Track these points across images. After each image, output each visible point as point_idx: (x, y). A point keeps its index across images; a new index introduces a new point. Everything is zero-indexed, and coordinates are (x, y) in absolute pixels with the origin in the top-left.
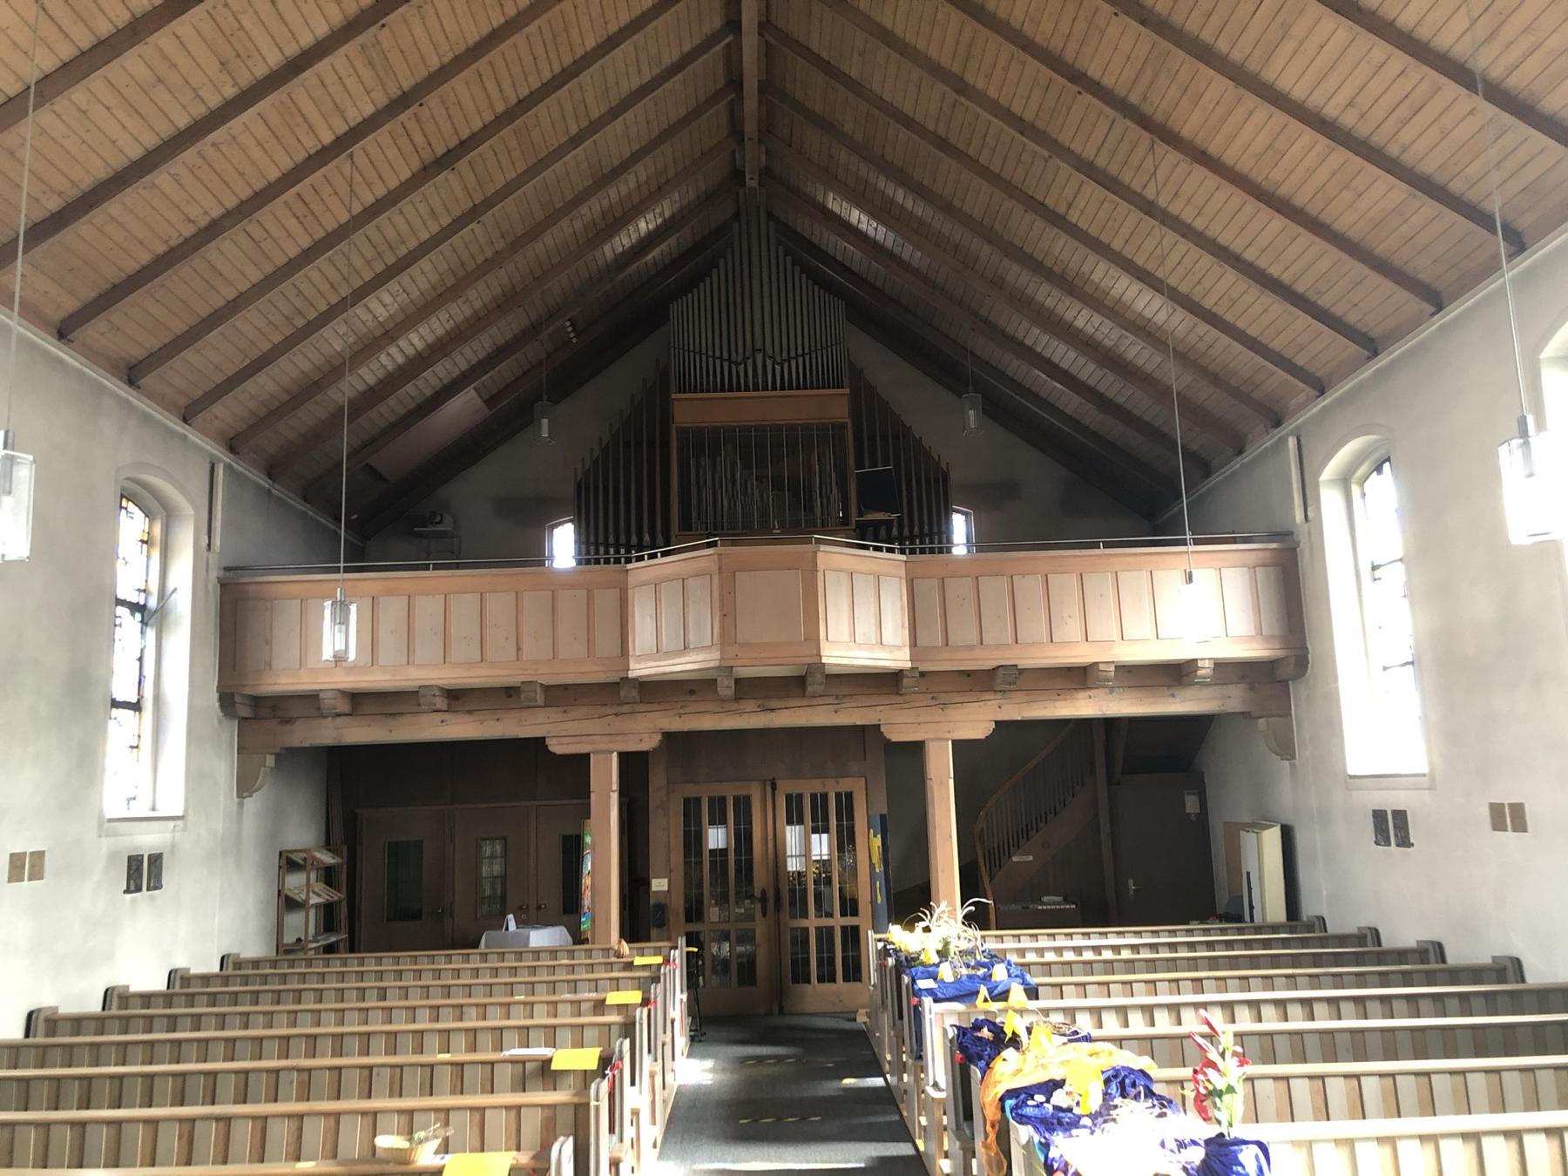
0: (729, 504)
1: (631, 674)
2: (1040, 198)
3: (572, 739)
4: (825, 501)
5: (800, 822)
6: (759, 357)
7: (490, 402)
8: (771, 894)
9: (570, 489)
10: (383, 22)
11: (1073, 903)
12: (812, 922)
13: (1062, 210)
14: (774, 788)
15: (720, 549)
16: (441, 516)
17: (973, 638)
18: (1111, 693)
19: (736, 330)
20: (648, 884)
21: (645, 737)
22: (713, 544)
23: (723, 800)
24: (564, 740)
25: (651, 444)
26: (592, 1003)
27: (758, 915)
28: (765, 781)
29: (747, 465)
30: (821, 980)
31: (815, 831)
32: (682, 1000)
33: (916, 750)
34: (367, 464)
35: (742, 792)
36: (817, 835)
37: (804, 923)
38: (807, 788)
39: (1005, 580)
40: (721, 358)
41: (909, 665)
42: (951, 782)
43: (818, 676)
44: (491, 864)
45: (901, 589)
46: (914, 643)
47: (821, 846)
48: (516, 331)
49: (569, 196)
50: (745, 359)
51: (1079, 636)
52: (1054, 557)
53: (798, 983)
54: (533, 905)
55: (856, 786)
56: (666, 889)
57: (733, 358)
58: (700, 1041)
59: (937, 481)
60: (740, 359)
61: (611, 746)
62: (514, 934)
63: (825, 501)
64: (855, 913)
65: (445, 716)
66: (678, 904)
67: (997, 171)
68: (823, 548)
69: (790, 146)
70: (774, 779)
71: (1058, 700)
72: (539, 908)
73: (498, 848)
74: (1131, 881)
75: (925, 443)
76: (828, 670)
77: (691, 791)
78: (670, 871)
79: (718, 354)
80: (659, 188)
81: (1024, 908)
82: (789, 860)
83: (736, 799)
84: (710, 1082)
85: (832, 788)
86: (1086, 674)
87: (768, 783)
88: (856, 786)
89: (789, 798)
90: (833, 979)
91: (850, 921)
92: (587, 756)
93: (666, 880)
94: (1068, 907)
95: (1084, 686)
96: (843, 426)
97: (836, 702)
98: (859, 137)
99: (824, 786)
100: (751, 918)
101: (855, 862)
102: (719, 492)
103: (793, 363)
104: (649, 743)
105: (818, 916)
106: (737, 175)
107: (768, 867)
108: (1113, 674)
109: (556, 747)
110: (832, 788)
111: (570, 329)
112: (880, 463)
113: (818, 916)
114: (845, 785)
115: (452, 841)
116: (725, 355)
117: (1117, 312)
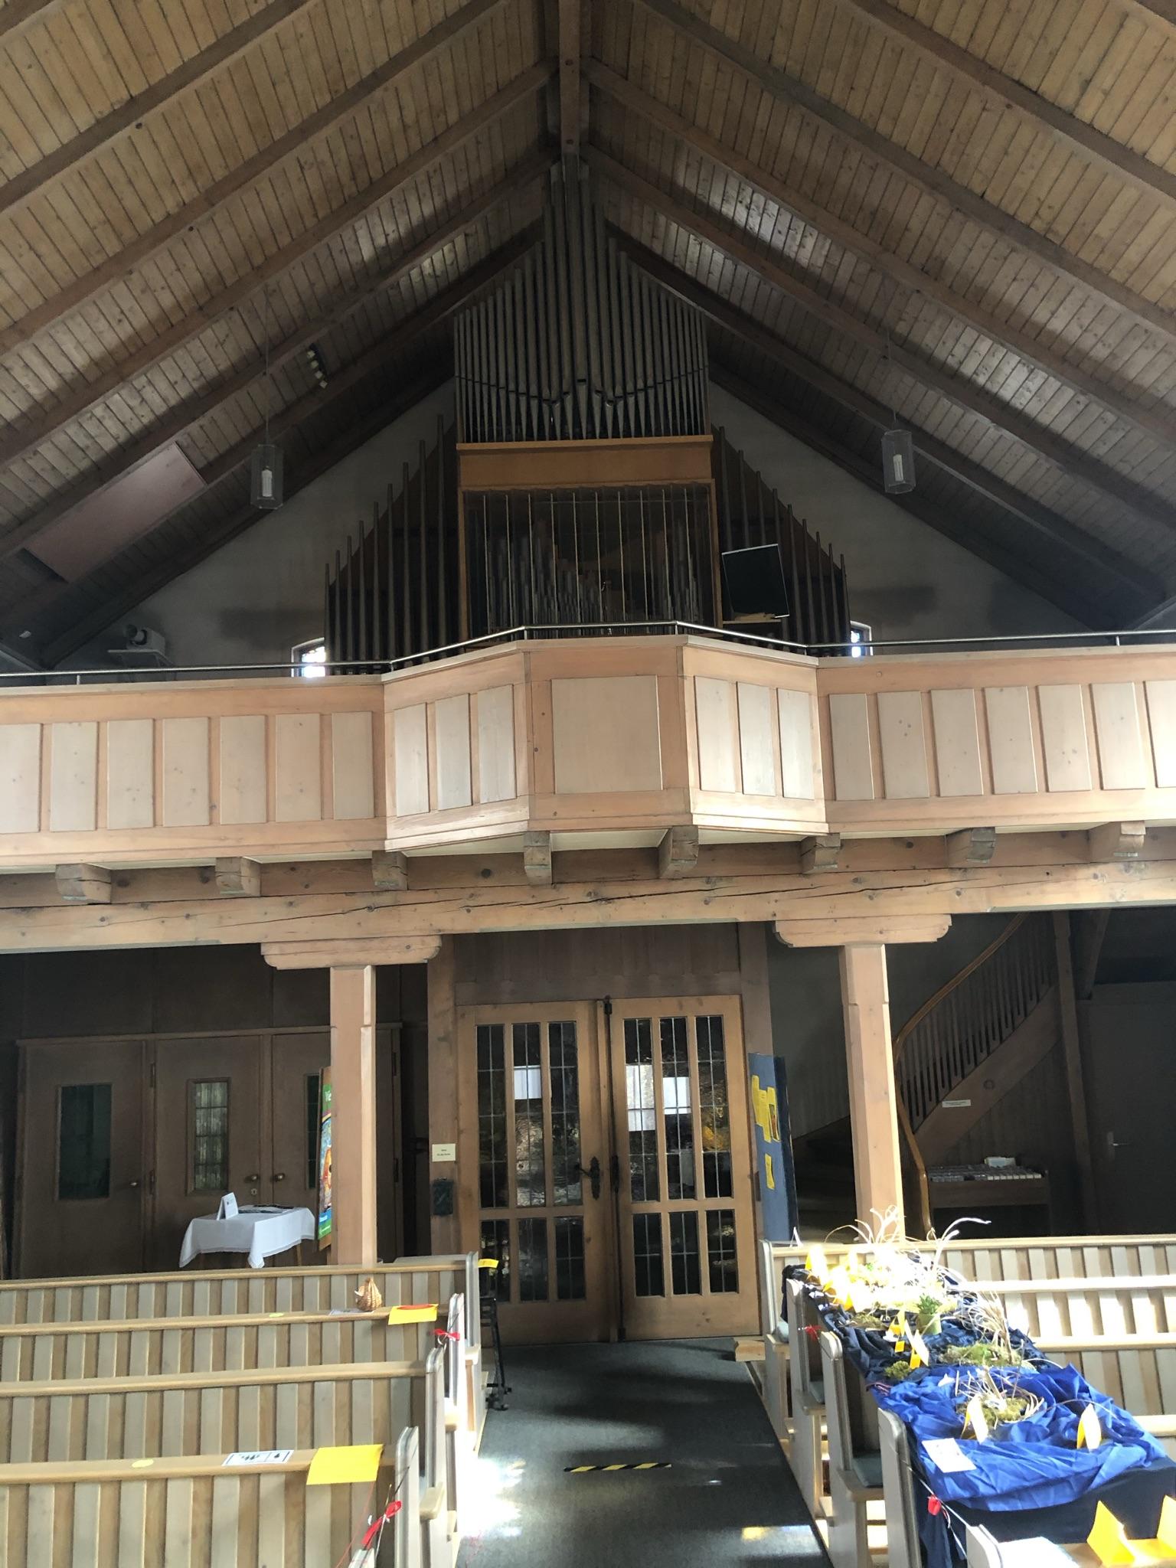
0: (541, 603)
1: (390, 846)
2: (1032, 82)
3: (308, 946)
4: (678, 600)
5: (646, 1057)
6: (582, 390)
7: (206, 471)
8: (605, 1166)
9: (318, 600)
10: (140, 120)
11: (1038, 1172)
12: (665, 1206)
13: (1067, 100)
14: (608, 1010)
15: (527, 643)
16: (145, 632)
17: (925, 788)
18: (1127, 871)
19: (546, 303)
20: (427, 1152)
21: (416, 943)
22: (520, 636)
23: (534, 1029)
24: (289, 948)
25: (432, 531)
26: (283, 1478)
27: (588, 1196)
28: (596, 1000)
29: (565, 553)
30: (679, 1290)
31: (670, 1072)
32: (469, 1364)
33: (832, 957)
34: (24, 551)
35: (561, 1017)
36: (672, 1079)
37: (653, 1207)
38: (656, 1010)
39: (973, 695)
40: (527, 394)
41: (824, 829)
42: (886, 1008)
43: (688, 847)
44: (208, 1116)
45: (811, 711)
46: (832, 794)
47: (678, 1095)
48: (234, 358)
49: (294, 122)
50: (562, 395)
51: (1090, 781)
52: (1044, 659)
53: (646, 1294)
54: (266, 1175)
55: (725, 1007)
56: (453, 1158)
57: (545, 393)
58: (503, 1409)
59: (827, 579)
60: (554, 395)
61: (361, 957)
62: (234, 1224)
63: (678, 600)
64: (727, 1191)
65: (107, 911)
66: (470, 1181)
67: (963, 44)
68: (693, 640)
69: (627, 79)
70: (608, 998)
71: (1046, 882)
72: (275, 1179)
73: (219, 1093)
74: (1110, 1136)
75: (811, 530)
76: (705, 839)
77: (490, 1016)
78: (460, 1132)
79: (522, 388)
80: (436, 139)
81: (966, 1179)
82: (630, 1115)
83: (555, 1028)
84: (515, 1532)
85: (692, 1010)
86: (1088, 839)
87: (600, 1004)
88: (725, 1007)
89: (629, 1025)
90: (696, 1289)
91: (720, 1203)
92: (326, 971)
93: (454, 1145)
94: (1030, 1177)
95: (1088, 860)
96: (703, 491)
97: (708, 887)
98: (733, 32)
99: (681, 1006)
100: (579, 1202)
101: (726, 1110)
102: (527, 587)
103: (631, 400)
104: (420, 952)
105: (674, 1195)
106: (549, 143)
107: (600, 1123)
108: (1142, 839)
109: (278, 959)
110: (692, 1010)
111: (315, 364)
112: (764, 538)
113: (674, 1195)
114: (710, 1007)
115: (153, 1084)
116: (534, 390)
117: (1129, 290)
